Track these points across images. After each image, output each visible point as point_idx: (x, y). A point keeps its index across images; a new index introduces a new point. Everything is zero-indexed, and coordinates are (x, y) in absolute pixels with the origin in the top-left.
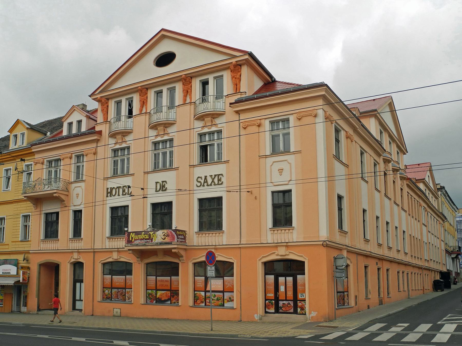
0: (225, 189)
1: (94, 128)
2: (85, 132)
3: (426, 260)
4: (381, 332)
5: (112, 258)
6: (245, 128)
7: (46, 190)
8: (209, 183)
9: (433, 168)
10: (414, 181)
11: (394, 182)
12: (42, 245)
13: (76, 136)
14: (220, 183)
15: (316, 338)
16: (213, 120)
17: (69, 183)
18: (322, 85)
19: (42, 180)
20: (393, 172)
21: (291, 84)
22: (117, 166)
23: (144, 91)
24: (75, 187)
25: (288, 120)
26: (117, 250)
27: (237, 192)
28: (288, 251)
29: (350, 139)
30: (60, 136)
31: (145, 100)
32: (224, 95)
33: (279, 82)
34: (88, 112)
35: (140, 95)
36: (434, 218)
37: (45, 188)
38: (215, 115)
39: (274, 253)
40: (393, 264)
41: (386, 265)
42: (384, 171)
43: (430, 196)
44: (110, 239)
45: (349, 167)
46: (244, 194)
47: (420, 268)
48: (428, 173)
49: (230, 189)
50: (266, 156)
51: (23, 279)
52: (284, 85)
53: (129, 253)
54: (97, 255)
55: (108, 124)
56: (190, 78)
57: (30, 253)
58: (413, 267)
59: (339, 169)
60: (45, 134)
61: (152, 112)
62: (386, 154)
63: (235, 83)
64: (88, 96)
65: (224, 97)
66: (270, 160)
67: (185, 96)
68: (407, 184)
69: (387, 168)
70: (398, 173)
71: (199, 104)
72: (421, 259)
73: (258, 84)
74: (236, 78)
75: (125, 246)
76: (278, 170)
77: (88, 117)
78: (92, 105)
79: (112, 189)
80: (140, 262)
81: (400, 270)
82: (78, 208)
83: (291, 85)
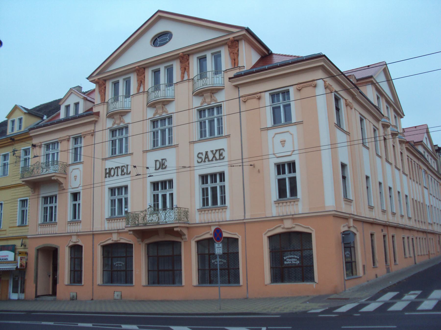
0: (227, 163)
1: (92, 109)
2: (83, 114)
3: (429, 223)
4: (369, 302)
5: (112, 239)
6: (245, 102)
7: (44, 173)
8: (210, 159)
9: (430, 130)
10: (413, 143)
11: (394, 146)
12: (40, 229)
13: (73, 118)
14: (221, 157)
15: (330, 311)
16: (212, 95)
17: (67, 166)
18: (320, 56)
19: (40, 164)
20: (392, 136)
21: (288, 56)
22: (115, 146)
23: (141, 71)
24: (73, 169)
25: (288, 92)
26: (116, 231)
27: (240, 166)
28: (295, 223)
29: (350, 106)
30: (57, 119)
31: (142, 79)
32: (222, 70)
33: (276, 54)
34: (84, 93)
35: (137, 75)
36: (438, 183)
37: (44, 172)
38: (214, 91)
39: (280, 226)
40: (398, 230)
41: (392, 232)
42: (383, 136)
43: (429, 158)
44: (109, 220)
45: (351, 135)
46: (247, 168)
47: (424, 232)
48: (426, 135)
49: (233, 162)
50: (268, 129)
51: (20, 264)
52: (281, 57)
53: (130, 234)
54: (96, 237)
55: (106, 105)
56: (188, 56)
57: (28, 238)
58: (418, 231)
59: (341, 137)
60: (42, 118)
61: (150, 91)
62: (383, 120)
63: (233, 58)
64: (86, 78)
65: (223, 72)
66: (271, 133)
67: (183, 74)
68: (407, 148)
69: (386, 133)
70: (397, 137)
71: (198, 80)
72: (424, 223)
73: (255, 58)
74: (234, 53)
75: (126, 227)
76: (281, 142)
77: (85, 99)
78: (88, 86)
79: (110, 169)
80: (141, 243)
81: (405, 236)
82: (75, 191)
83: (288, 57)
